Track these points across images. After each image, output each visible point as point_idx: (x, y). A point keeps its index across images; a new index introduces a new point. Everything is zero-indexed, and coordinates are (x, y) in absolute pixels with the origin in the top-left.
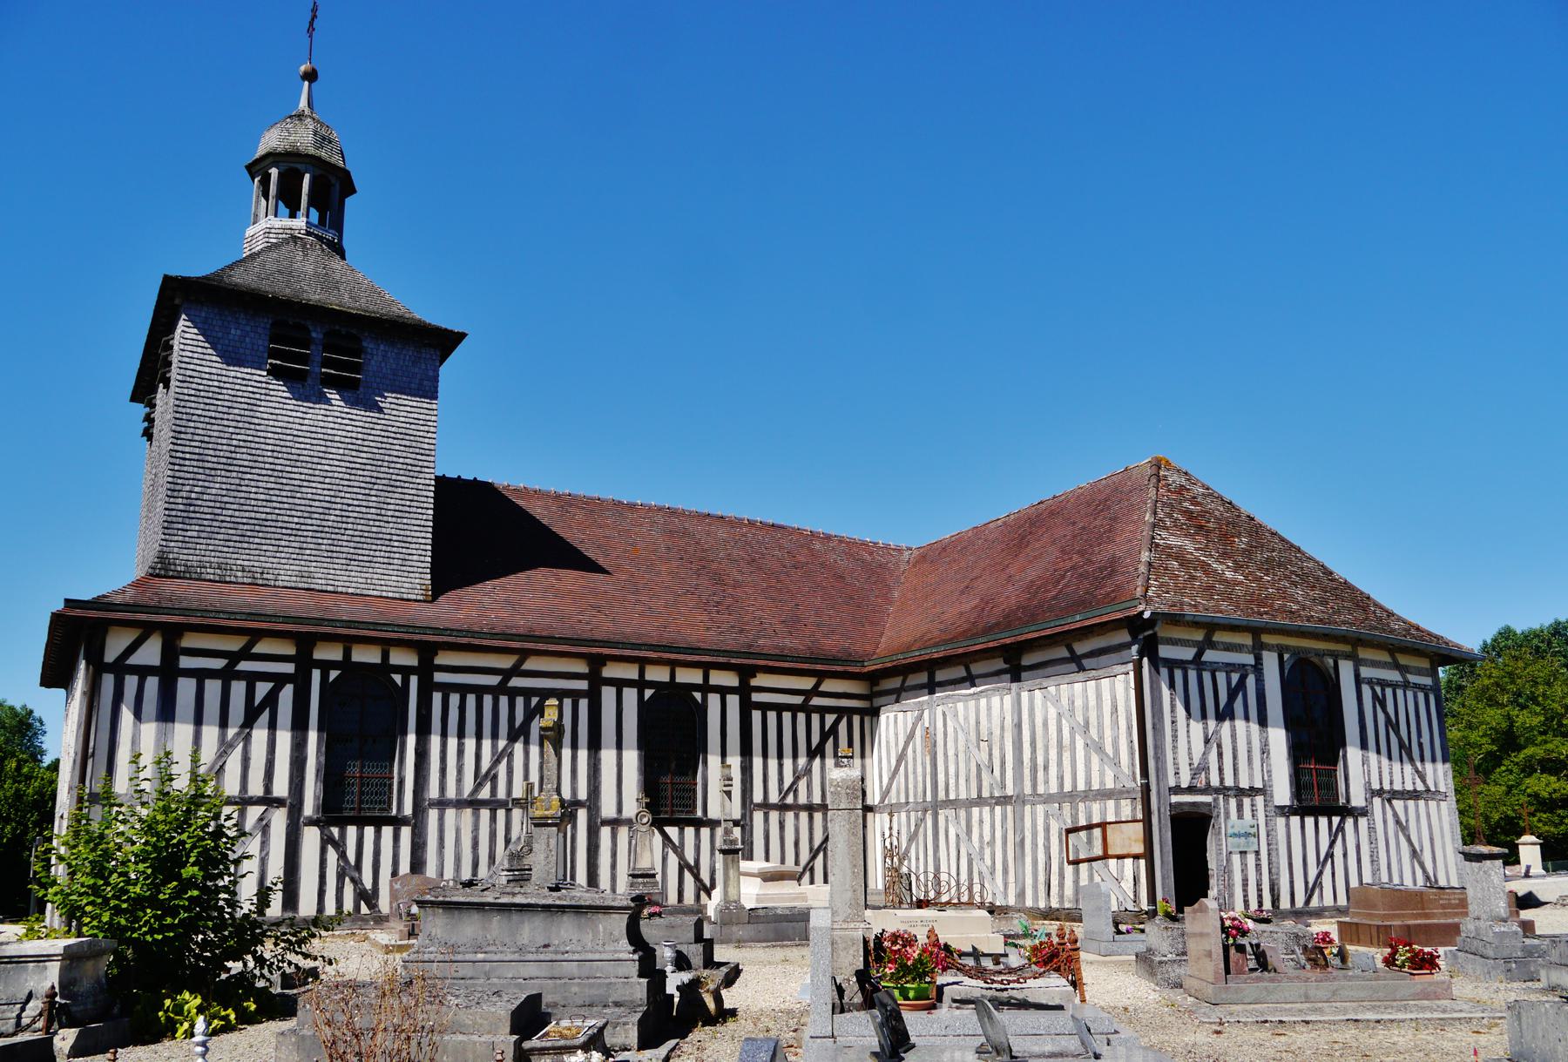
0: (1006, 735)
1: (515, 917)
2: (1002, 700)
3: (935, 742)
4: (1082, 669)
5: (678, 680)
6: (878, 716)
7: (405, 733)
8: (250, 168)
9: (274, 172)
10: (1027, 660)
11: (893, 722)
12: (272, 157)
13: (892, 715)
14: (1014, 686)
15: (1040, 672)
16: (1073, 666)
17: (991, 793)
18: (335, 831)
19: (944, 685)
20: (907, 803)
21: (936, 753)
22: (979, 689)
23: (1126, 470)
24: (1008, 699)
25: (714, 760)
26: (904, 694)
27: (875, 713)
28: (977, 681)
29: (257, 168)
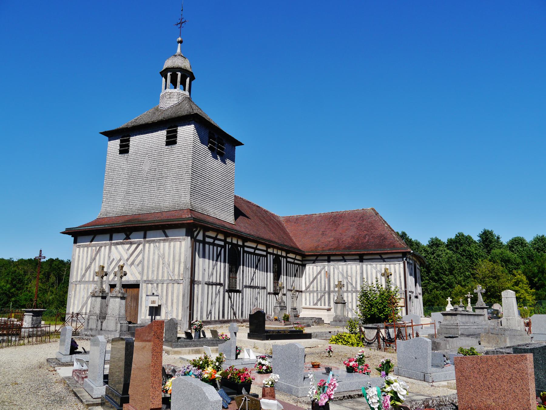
0: (358, 275)
1: (470, 316)
2: (356, 266)
3: (330, 275)
4: (384, 261)
5: (256, 252)
6: (305, 267)
7: (240, 265)
8: (161, 73)
9: (169, 74)
10: (365, 257)
11: (311, 269)
12: (168, 70)
13: (311, 267)
14: (361, 263)
15: (370, 261)
16: (382, 261)
17: (352, 290)
18: (230, 294)
19: (333, 261)
20: (317, 291)
21: (330, 278)
22: (347, 263)
23: (363, 209)
24: (358, 267)
25: (282, 276)
26: (316, 261)
27: (304, 266)
28: (364, 261)
29: (164, 74)
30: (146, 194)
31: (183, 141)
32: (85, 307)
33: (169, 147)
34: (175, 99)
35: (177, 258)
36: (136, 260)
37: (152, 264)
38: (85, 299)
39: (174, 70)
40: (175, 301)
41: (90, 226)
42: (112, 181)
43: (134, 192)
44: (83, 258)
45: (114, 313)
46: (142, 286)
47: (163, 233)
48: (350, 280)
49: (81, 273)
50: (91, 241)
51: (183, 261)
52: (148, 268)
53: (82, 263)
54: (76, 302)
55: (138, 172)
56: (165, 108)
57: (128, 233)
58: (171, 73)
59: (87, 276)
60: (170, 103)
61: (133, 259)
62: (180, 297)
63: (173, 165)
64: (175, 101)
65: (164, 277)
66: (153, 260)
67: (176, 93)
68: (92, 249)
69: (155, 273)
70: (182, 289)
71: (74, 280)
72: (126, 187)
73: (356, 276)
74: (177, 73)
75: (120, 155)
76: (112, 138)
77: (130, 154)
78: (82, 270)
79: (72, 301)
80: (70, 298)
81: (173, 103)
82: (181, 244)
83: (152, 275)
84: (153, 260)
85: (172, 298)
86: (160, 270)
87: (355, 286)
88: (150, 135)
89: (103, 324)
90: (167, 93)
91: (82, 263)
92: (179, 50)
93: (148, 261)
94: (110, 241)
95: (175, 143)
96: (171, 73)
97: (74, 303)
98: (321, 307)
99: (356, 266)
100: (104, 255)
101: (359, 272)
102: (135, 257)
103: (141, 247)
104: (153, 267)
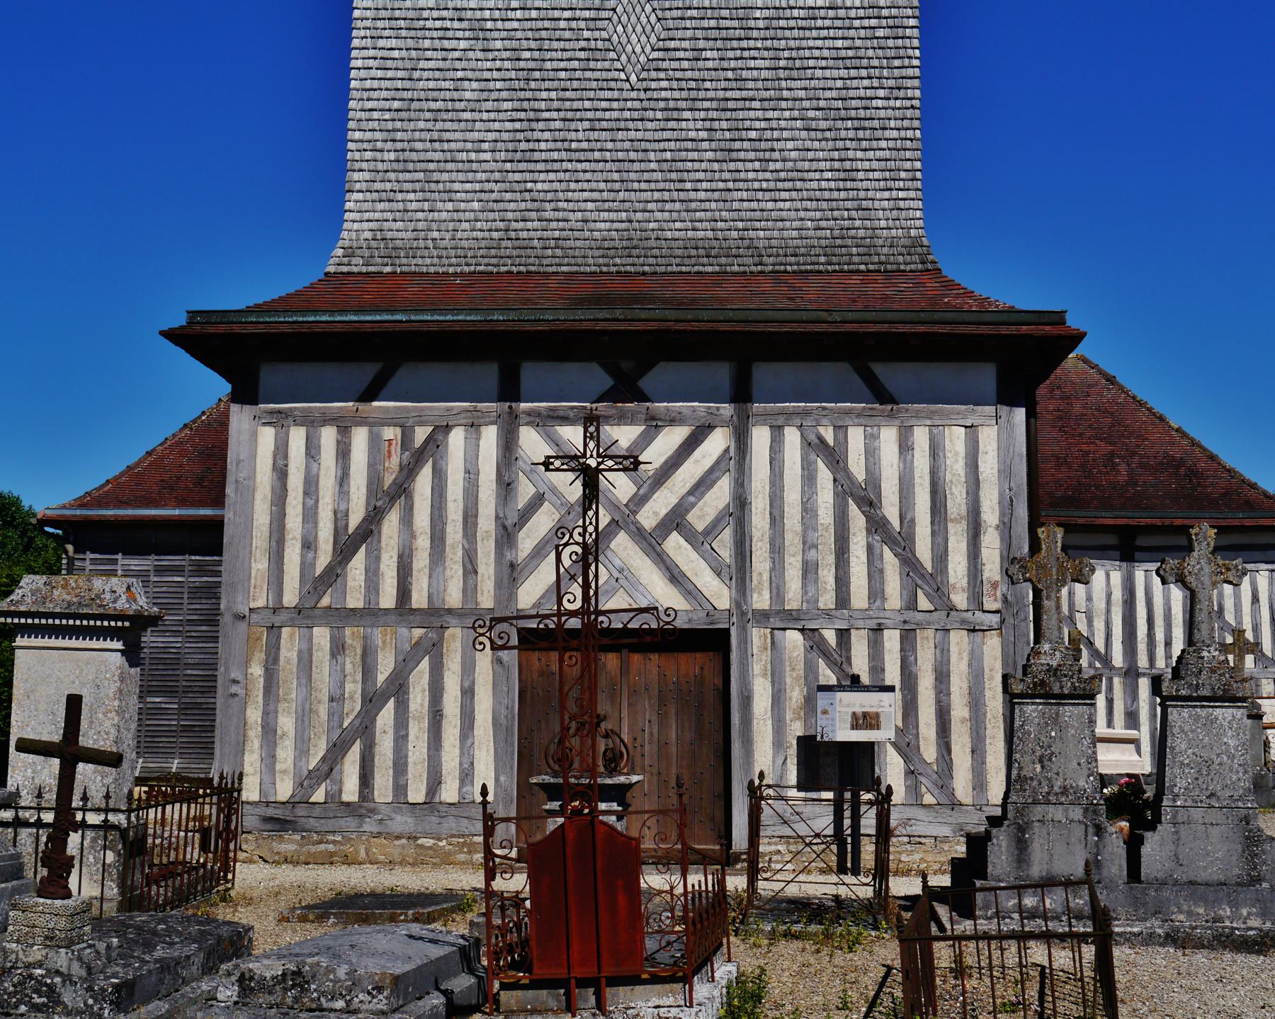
10: (1141, 541)
14: (1124, 564)
24: (1117, 577)
35: (957, 501)
36: (693, 505)
37: (799, 528)
40: (960, 710)
41: (295, 312)
42: (407, 84)
43: (564, 155)
44: (311, 487)
45: (1215, 786)
46: (745, 641)
47: (857, 380)
48: (1082, 626)
49: (306, 567)
51: (996, 522)
52: (777, 550)
53: (310, 515)
57: (626, 365)
59: (350, 584)
61: (674, 501)
62: (988, 694)
65: (884, 599)
68: (374, 441)
69: (828, 576)
71: (261, 603)
72: (509, 126)
73: (1108, 611)
78: (309, 545)
79: (254, 715)
80: (235, 703)
83: (804, 586)
85: (938, 702)
86: (853, 561)
89: (1146, 850)
91: (310, 515)
98: (1110, 731)
99: (1108, 575)
100: (471, 474)
101: (1117, 595)
102: (691, 492)
103: (717, 443)
104: (808, 545)
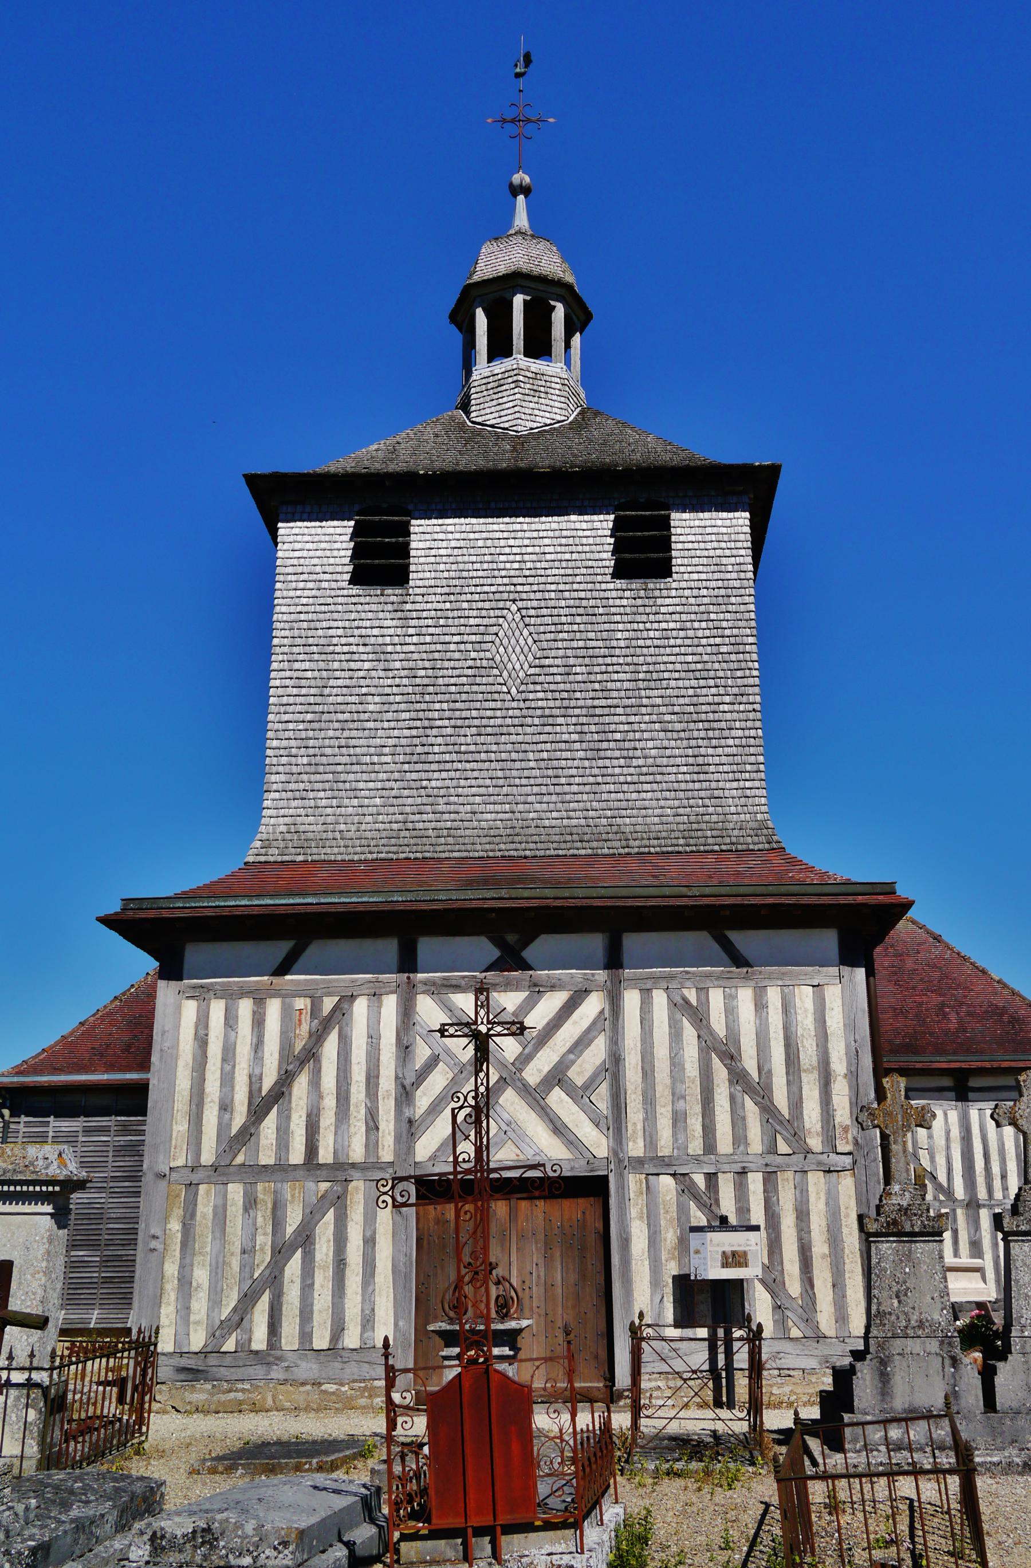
9: (519, 301)
10: (973, 1082)
14: (959, 1104)
24: (953, 1116)
30: (526, 773)
31: (700, 568)
32: (266, 1298)
33: (634, 586)
34: (557, 404)
35: (808, 1053)
38: (264, 1257)
39: (541, 287)
40: (820, 1248)
42: (319, 699)
46: (622, 1186)
48: (926, 1163)
49: (223, 1127)
50: (282, 969)
52: (649, 1101)
53: (227, 1080)
54: (201, 1275)
55: (470, 672)
56: (519, 428)
57: (511, 938)
58: (528, 298)
59: (263, 1142)
60: (537, 412)
62: (845, 1230)
63: (660, 659)
64: (555, 410)
66: (676, 1063)
67: (558, 380)
68: (287, 1012)
69: (695, 1124)
70: (853, 1192)
71: (180, 1162)
72: (407, 733)
73: (948, 1148)
74: (552, 303)
75: (355, 590)
76: (299, 508)
77: (674, 585)
78: (226, 1107)
79: (171, 1269)
81: (548, 415)
82: (823, 999)
84: (676, 1063)
85: (800, 1239)
87: (945, 1185)
88: (498, 525)
89: (999, 1380)
90: (522, 373)
92: (521, 219)
93: (648, 1072)
94: (401, 970)
95: (663, 569)
96: (528, 298)
97: (185, 1283)
98: (957, 1260)
100: (374, 1039)
101: (955, 1132)
102: (570, 1051)
103: (593, 1005)
104: (677, 1096)
